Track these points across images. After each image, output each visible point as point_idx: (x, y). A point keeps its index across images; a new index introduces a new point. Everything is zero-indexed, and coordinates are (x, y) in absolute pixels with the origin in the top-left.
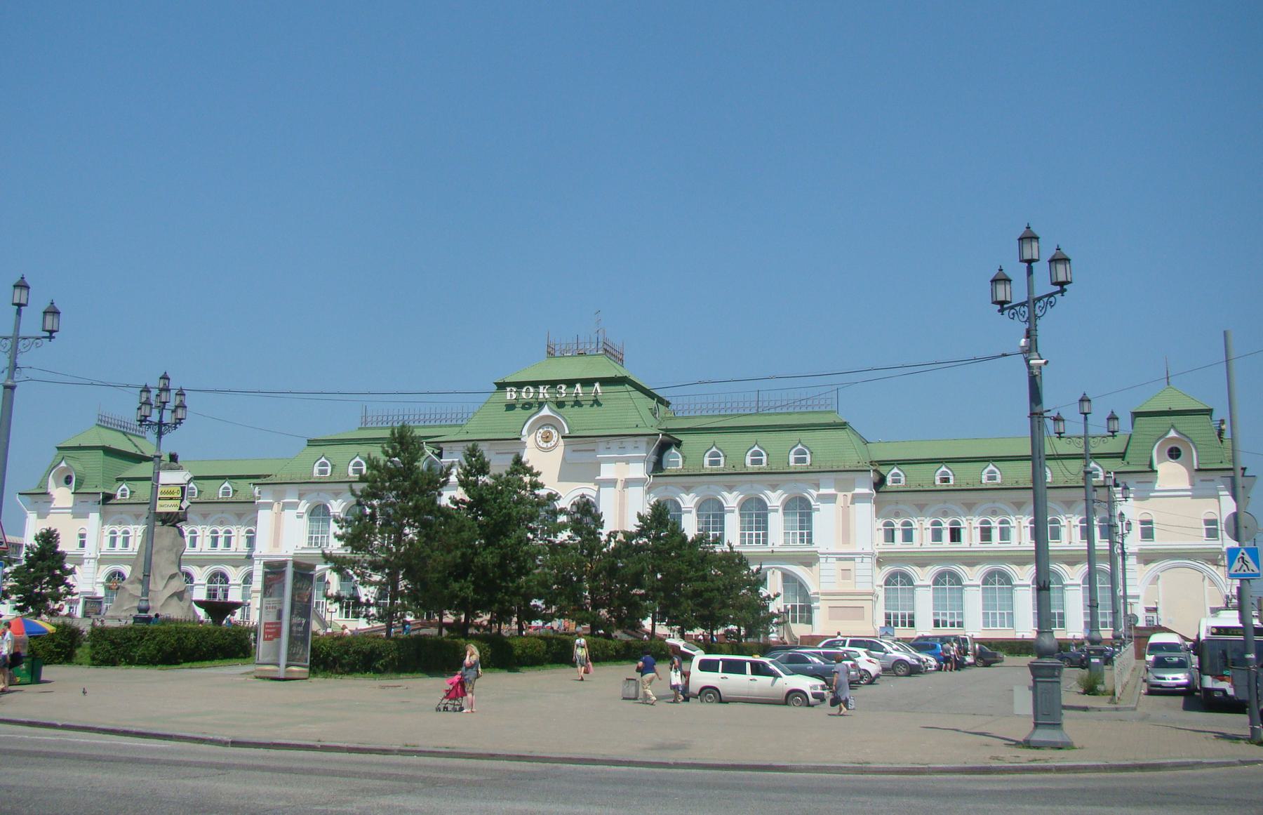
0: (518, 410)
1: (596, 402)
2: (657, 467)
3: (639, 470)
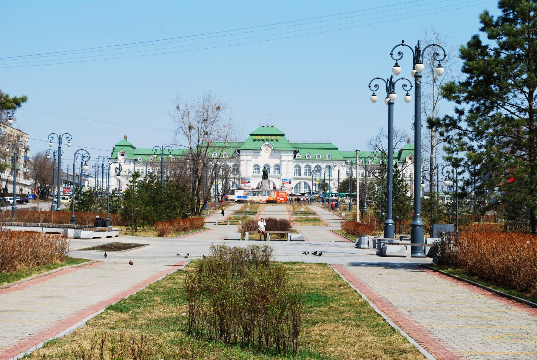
0: (257, 141)
1: (277, 140)
2: (295, 157)
3: (291, 158)
